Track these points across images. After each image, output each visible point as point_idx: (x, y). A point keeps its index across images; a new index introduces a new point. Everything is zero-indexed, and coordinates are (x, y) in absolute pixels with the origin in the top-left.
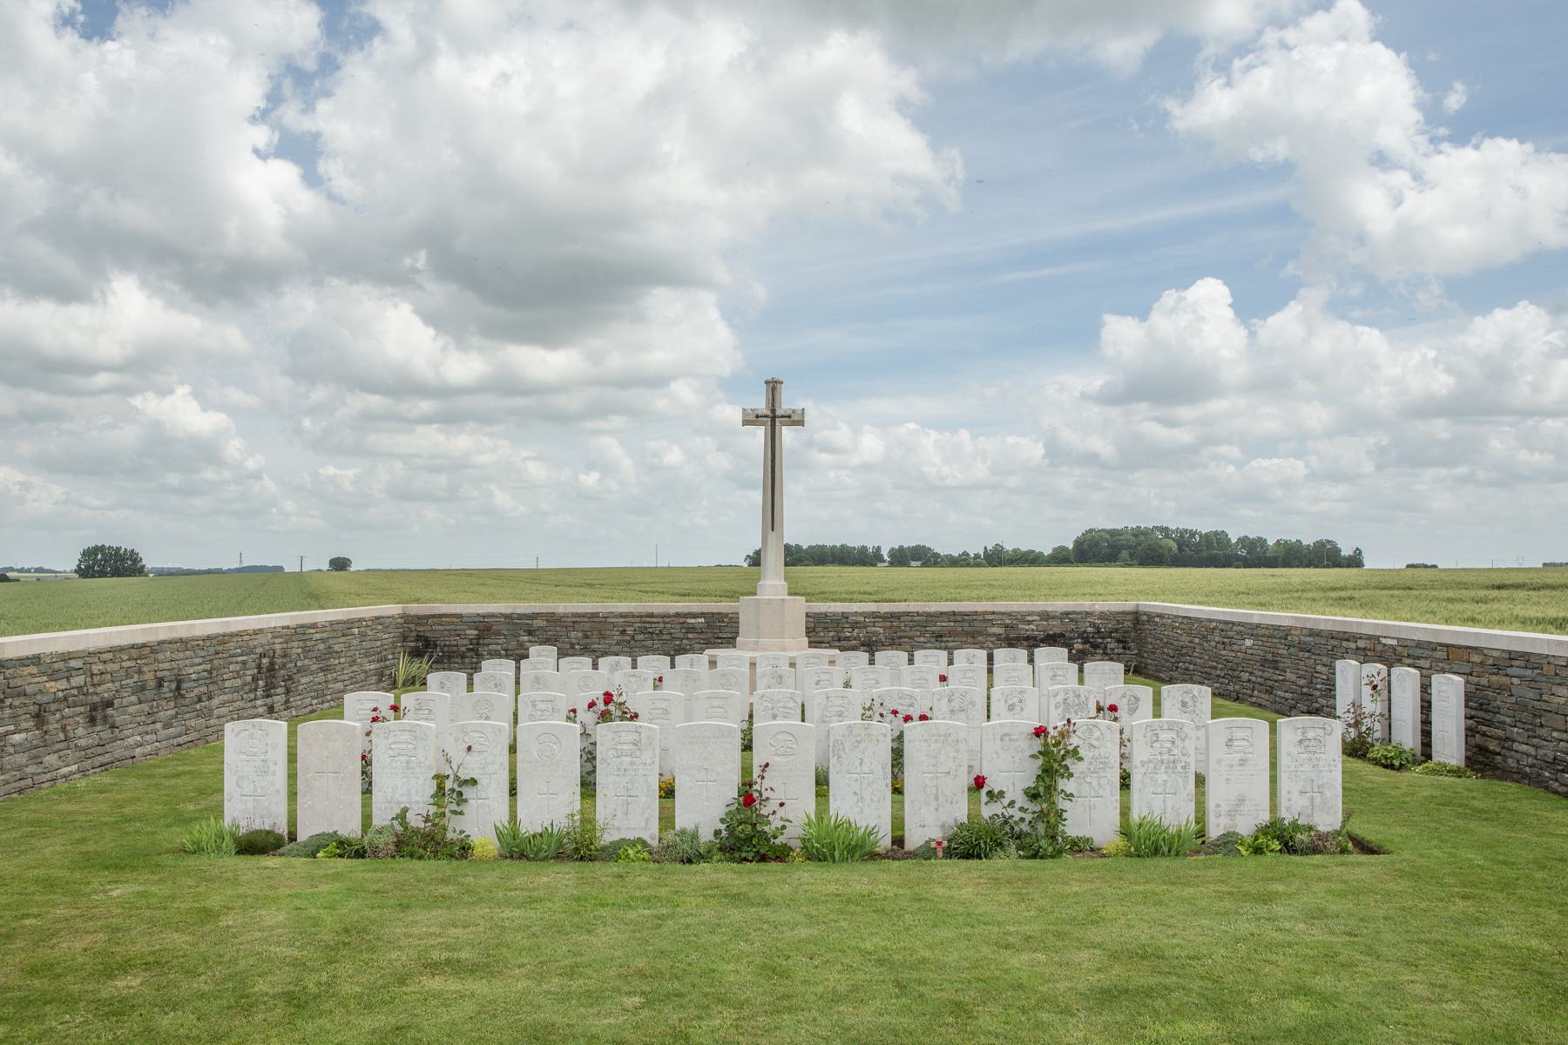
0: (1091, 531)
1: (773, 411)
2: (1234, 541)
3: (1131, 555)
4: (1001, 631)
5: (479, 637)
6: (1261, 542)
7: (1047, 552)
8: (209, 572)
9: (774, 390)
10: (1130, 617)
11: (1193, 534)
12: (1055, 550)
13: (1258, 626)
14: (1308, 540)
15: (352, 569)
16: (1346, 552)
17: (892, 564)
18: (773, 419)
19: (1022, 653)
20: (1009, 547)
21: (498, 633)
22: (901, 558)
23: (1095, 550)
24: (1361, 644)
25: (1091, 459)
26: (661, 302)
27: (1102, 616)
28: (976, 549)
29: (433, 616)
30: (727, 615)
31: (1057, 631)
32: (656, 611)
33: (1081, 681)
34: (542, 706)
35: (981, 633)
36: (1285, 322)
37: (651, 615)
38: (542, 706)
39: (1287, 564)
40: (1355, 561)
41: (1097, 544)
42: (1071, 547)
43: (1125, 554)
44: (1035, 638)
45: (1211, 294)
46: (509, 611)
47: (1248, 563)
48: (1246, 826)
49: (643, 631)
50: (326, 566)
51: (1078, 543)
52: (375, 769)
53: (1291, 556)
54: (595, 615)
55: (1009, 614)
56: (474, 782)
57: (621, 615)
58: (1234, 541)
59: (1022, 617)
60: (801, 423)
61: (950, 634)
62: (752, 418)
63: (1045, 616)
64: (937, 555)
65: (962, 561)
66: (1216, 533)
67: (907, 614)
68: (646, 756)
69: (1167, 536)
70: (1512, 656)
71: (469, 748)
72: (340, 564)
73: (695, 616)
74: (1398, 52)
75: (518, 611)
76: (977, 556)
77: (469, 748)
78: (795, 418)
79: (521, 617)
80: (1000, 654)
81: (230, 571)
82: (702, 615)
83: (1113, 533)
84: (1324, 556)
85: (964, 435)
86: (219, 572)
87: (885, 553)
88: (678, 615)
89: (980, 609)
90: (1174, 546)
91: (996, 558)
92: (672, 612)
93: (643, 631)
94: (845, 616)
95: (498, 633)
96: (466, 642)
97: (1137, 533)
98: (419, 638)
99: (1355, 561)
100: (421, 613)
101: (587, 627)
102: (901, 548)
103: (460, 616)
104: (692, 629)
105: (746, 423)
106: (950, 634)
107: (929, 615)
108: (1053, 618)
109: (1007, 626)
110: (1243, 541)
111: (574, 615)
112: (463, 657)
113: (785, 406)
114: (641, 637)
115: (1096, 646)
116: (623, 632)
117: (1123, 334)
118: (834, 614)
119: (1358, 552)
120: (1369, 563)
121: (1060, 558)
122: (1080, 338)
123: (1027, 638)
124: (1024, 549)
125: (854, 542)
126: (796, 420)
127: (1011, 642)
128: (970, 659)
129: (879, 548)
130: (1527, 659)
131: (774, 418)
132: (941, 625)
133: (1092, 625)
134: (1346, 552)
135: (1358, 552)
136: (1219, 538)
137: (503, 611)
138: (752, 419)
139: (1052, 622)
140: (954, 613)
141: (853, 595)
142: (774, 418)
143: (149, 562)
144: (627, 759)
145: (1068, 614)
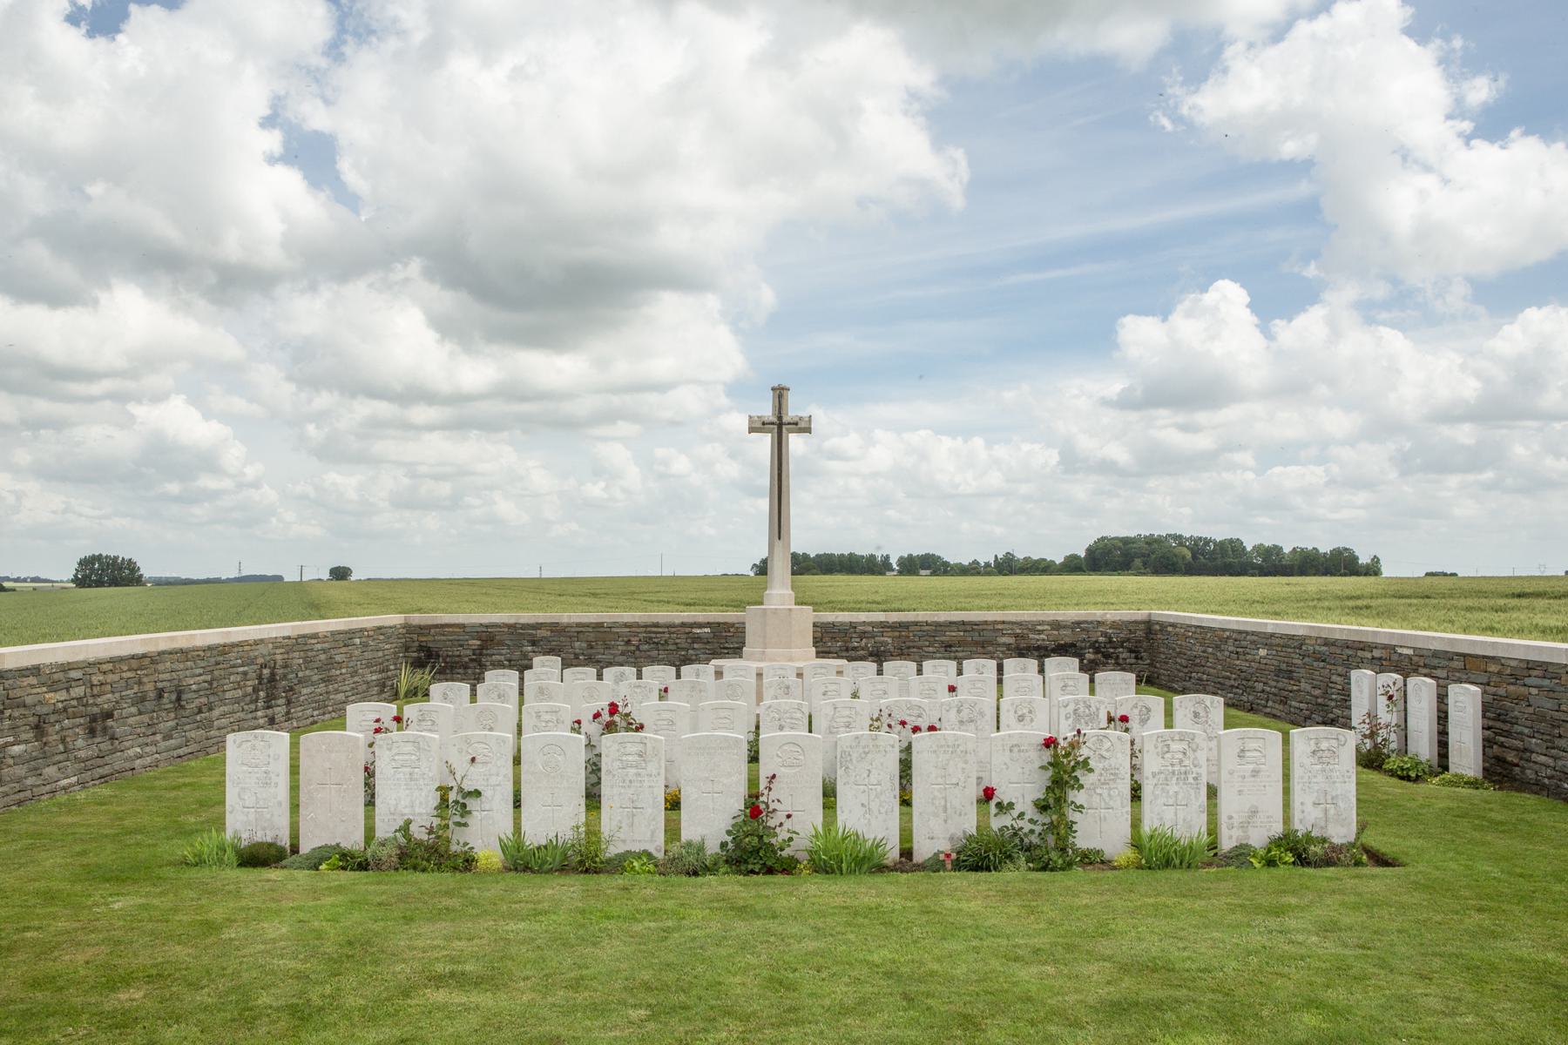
0: (1103, 539)
1: (780, 418)
3: (1145, 564)
4: (1011, 640)
5: (482, 648)
6: (1277, 550)
7: (1059, 560)
8: (207, 581)
9: (780, 397)
10: (1142, 626)
11: (1207, 542)
12: (1067, 558)
14: (1325, 548)
15: (353, 578)
16: (1364, 559)
17: (901, 573)
18: (779, 426)
19: (1033, 664)
20: (1020, 555)
21: (501, 643)
22: (911, 566)
23: (1109, 557)
24: (1377, 653)
25: (1106, 467)
26: (669, 306)
29: (436, 626)
30: (733, 625)
31: (1068, 640)
37: (656, 625)
38: (548, 717)
40: (1373, 570)
41: (1110, 552)
42: (1083, 554)
43: (1138, 562)
44: (1046, 648)
45: (1229, 296)
46: (512, 621)
48: (1258, 838)
49: (648, 641)
50: (326, 576)
51: (1090, 551)
53: (1308, 564)
54: (600, 625)
55: (1020, 624)
56: (477, 793)
57: (626, 625)
59: (1032, 627)
60: (808, 430)
62: (759, 425)
63: (1056, 625)
64: (946, 564)
65: (972, 570)
66: (1231, 541)
67: (916, 624)
68: (652, 767)
69: (1181, 544)
70: (1530, 666)
71: (473, 760)
72: (340, 574)
73: (700, 626)
76: (987, 565)
77: (473, 760)
78: (802, 425)
79: (525, 626)
80: (1010, 664)
81: (229, 581)
82: (708, 625)
84: (1341, 563)
85: (978, 442)
86: (217, 581)
88: (683, 625)
89: (990, 619)
90: (1189, 555)
91: (1007, 566)
92: (677, 621)
93: (648, 641)
94: (853, 625)
97: (1151, 541)
98: (421, 648)
103: (463, 626)
104: (697, 639)
105: (752, 430)
106: (961, 643)
107: (938, 624)
108: (1065, 627)
109: (1017, 636)
110: (1259, 549)
111: (579, 625)
112: (466, 667)
113: (792, 413)
116: (628, 642)
117: (1141, 335)
118: (842, 624)
119: (1376, 560)
120: (1387, 571)
121: (1073, 566)
122: (1094, 339)
123: (1038, 648)
125: (862, 551)
126: (758, 426)
127: (1021, 652)
128: (980, 670)
129: (888, 557)
132: (952, 635)
133: (1105, 634)
135: (1376, 560)
136: (1234, 546)
138: (758, 426)
139: (1063, 632)
140: (964, 623)
142: (780, 425)
143: (147, 571)
144: (633, 771)
145: (1078, 623)
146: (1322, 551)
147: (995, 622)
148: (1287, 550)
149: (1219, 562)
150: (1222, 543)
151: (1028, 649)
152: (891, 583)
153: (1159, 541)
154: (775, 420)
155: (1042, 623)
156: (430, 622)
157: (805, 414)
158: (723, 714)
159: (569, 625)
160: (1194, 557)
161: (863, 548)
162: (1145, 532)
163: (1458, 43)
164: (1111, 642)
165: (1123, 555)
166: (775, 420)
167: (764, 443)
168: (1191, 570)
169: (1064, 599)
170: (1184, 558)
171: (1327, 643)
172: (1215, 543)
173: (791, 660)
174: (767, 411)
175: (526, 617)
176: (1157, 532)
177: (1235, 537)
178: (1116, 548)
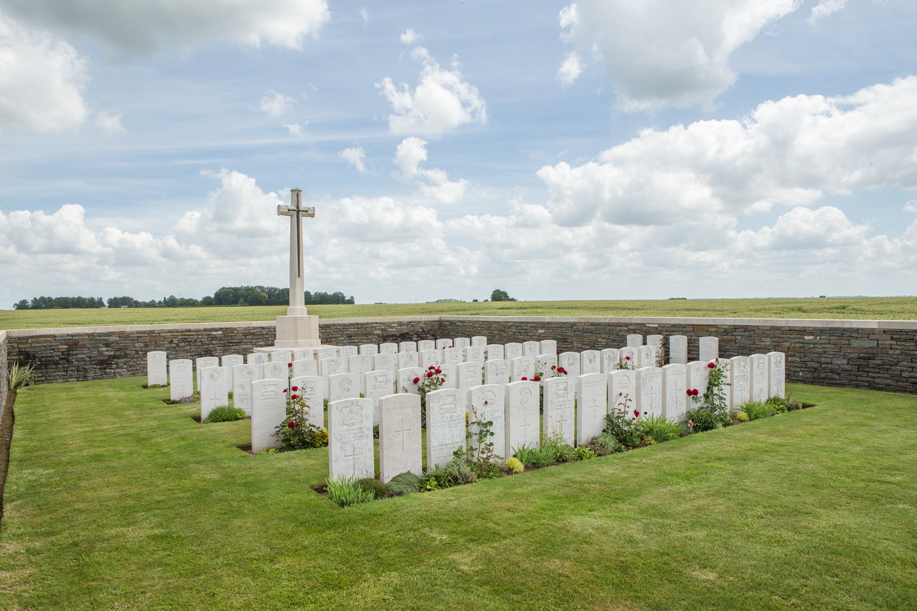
0: (223, 288)
1: (298, 207)
3: (245, 301)
4: (380, 332)
5: (69, 350)
7: (200, 299)
11: (275, 290)
13: (548, 323)
14: (330, 292)
16: (347, 298)
17: (110, 307)
20: (178, 297)
21: (84, 346)
22: (115, 303)
23: (227, 298)
27: (425, 323)
28: (159, 299)
29: (33, 337)
30: (235, 329)
31: (406, 331)
32: (192, 328)
33: (220, 365)
34: (380, 379)
35: (370, 334)
37: (189, 331)
38: (380, 379)
39: (320, 303)
40: (351, 302)
41: (227, 295)
42: (213, 296)
43: (242, 300)
46: (91, 332)
51: (217, 295)
52: (420, 425)
54: (152, 332)
55: (384, 324)
56: (491, 423)
59: (389, 325)
60: (312, 216)
61: (356, 335)
63: (400, 324)
65: (152, 305)
67: (334, 325)
69: (263, 291)
70: (736, 328)
71: (486, 403)
73: (216, 330)
75: (98, 331)
76: (160, 302)
77: (486, 403)
79: (100, 335)
82: (220, 329)
83: (235, 289)
87: (30, 303)
88: (205, 330)
90: (267, 296)
91: (171, 303)
92: (202, 328)
95: (84, 346)
96: (58, 354)
97: (248, 289)
98: (20, 353)
99: (351, 302)
100: (21, 335)
101: (147, 339)
102: (115, 298)
103: (54, 336)
104: (215, 338)
106: (356, 335)
107: (345, 325)
109: (382, 330)
111: (138, 332)
112: (57, 364)
113: (304, 205)
116: (171, 342)
119: (352, 298)
121: (207, 302)
123: (392, 336)
124: (187, 298)
125: (86, 296)
130: (745, 328)
131: (298, 212)
132: (351, 331)
133: (421, 328)
134: (347, 298)
135: (352, 298)
137: (87, 332)
140: (357, 324)
141: (339, 316)
142: (298, 212)
147: (372, 323)
149: (281, 300)
151: (387, 336)
152: (106, 312)
154: (294, 208)
155: (393, 323)
156: (27, 335)
157: (311, 207)
158: (471, 369)
159: (132, 333)
160: (269, 297)
161: (86, 293)
163: (456, 55)
166: (294, 208)
167: (286, 223)
168: (269, 303)
169: (213, 318)
171: (592, 324)
173: (311, 345)
174: (288, 203)
175: (101, 329)
176: (253, 284)
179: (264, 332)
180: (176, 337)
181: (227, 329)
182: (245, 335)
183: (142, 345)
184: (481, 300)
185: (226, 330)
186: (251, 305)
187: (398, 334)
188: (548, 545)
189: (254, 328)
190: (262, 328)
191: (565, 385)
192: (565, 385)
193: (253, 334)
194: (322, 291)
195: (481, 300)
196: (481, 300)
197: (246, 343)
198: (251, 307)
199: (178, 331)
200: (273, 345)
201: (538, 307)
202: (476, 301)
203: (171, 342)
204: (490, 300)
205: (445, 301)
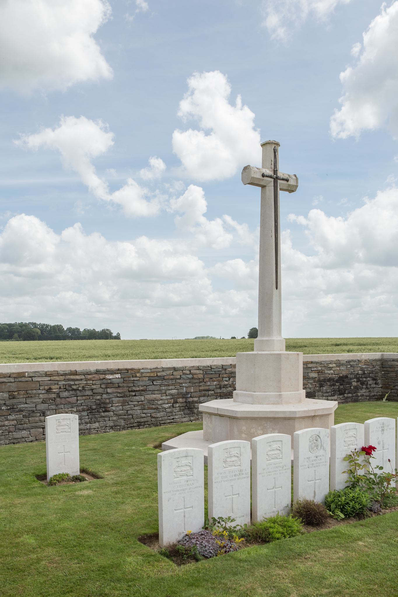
1: (275, 172)
2: (65, 329)
6: (77, 330)
10: (379, 363)
11: (47, 326)
14: (98, 329)
16: (114, 334)
27: (367, 362)
31: (344, 373)
32: (79, 369)
36: (68, 233)
37: (75, 373)
40: (118, 337)
43: (16, 335)
47: (71, 338)
53: (91, 335)
54: (21, 375)
55: (320, 363)
57: (46, 374)
58: (65, 329)
59: (326, 365)
63: (339, 364)
66: (58, 326)
69: (36, 327)
73: (112, 372)
74: (225, 75)
83: (10, 325)
84: (106, 335)
88: (98, 372)
90: (39, 332)
92: (93, 369)
97: (22, 325)
99: (118, 337)
101: (13, 387)
104: (110, 384)
109: (319, 372)
110: (70, 329)
114: (66, 394)
115: (362, 384)
116: (49, 391)
119: (119, 335)
120: (122, 338)
123: (330, 380)
126: (248, 177)
133: (362, 369)
134: (114, 334)
135: (119, 335)
136: (59, 328)
146: (97, 330)
148: (82, 330)
150: (54, 327)
151: (324, 380)
153: (26, 325)
154: (269, 172)
160: (42, 333)
162: (19, 322)
164: (364, 373)
165: (8, 331)
170: (37, 333)
172: (51, 327)
177: (59, 324)
178: (4, 328)
179: (177, 374)
180: (57, 382)
181: (127, 370)
182: (152, 380)
183: (6, 395)
184: (239, 338)
185: (126, 372)
186: (24, 340)
187: (336, 377)
188: (228, 550)
189: (164, 370)
190: (175, 369)
191: (175, 405)
192: (175, 405)
193: (163, 378)
194: (90, 327)
195: (239, 337)
196: (239, 337)
197: (153, 392)
198: (26, 342)
199: (58, 374)
200: (229, 395)
201: (377, 344)
202: (234, 338)
203: (49, 391)
204: (247, 337)
205: (203, 338)
